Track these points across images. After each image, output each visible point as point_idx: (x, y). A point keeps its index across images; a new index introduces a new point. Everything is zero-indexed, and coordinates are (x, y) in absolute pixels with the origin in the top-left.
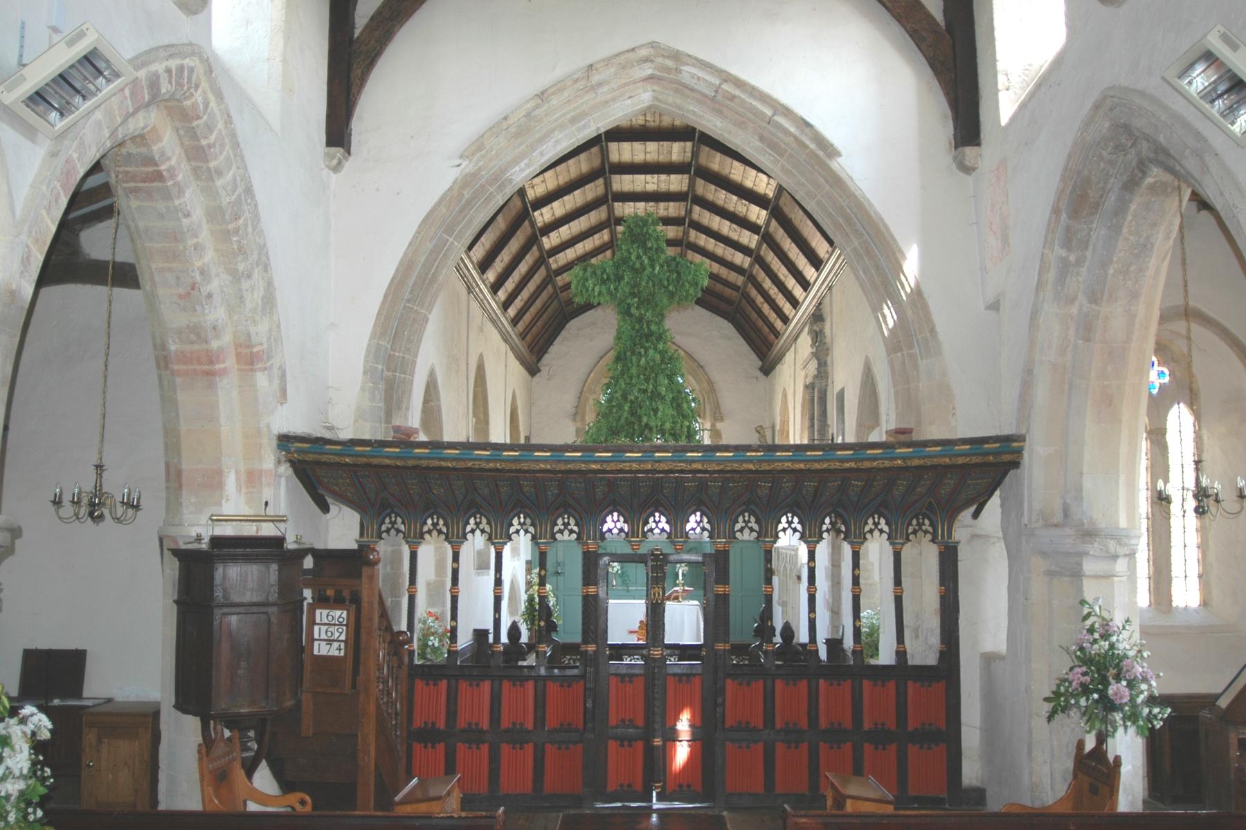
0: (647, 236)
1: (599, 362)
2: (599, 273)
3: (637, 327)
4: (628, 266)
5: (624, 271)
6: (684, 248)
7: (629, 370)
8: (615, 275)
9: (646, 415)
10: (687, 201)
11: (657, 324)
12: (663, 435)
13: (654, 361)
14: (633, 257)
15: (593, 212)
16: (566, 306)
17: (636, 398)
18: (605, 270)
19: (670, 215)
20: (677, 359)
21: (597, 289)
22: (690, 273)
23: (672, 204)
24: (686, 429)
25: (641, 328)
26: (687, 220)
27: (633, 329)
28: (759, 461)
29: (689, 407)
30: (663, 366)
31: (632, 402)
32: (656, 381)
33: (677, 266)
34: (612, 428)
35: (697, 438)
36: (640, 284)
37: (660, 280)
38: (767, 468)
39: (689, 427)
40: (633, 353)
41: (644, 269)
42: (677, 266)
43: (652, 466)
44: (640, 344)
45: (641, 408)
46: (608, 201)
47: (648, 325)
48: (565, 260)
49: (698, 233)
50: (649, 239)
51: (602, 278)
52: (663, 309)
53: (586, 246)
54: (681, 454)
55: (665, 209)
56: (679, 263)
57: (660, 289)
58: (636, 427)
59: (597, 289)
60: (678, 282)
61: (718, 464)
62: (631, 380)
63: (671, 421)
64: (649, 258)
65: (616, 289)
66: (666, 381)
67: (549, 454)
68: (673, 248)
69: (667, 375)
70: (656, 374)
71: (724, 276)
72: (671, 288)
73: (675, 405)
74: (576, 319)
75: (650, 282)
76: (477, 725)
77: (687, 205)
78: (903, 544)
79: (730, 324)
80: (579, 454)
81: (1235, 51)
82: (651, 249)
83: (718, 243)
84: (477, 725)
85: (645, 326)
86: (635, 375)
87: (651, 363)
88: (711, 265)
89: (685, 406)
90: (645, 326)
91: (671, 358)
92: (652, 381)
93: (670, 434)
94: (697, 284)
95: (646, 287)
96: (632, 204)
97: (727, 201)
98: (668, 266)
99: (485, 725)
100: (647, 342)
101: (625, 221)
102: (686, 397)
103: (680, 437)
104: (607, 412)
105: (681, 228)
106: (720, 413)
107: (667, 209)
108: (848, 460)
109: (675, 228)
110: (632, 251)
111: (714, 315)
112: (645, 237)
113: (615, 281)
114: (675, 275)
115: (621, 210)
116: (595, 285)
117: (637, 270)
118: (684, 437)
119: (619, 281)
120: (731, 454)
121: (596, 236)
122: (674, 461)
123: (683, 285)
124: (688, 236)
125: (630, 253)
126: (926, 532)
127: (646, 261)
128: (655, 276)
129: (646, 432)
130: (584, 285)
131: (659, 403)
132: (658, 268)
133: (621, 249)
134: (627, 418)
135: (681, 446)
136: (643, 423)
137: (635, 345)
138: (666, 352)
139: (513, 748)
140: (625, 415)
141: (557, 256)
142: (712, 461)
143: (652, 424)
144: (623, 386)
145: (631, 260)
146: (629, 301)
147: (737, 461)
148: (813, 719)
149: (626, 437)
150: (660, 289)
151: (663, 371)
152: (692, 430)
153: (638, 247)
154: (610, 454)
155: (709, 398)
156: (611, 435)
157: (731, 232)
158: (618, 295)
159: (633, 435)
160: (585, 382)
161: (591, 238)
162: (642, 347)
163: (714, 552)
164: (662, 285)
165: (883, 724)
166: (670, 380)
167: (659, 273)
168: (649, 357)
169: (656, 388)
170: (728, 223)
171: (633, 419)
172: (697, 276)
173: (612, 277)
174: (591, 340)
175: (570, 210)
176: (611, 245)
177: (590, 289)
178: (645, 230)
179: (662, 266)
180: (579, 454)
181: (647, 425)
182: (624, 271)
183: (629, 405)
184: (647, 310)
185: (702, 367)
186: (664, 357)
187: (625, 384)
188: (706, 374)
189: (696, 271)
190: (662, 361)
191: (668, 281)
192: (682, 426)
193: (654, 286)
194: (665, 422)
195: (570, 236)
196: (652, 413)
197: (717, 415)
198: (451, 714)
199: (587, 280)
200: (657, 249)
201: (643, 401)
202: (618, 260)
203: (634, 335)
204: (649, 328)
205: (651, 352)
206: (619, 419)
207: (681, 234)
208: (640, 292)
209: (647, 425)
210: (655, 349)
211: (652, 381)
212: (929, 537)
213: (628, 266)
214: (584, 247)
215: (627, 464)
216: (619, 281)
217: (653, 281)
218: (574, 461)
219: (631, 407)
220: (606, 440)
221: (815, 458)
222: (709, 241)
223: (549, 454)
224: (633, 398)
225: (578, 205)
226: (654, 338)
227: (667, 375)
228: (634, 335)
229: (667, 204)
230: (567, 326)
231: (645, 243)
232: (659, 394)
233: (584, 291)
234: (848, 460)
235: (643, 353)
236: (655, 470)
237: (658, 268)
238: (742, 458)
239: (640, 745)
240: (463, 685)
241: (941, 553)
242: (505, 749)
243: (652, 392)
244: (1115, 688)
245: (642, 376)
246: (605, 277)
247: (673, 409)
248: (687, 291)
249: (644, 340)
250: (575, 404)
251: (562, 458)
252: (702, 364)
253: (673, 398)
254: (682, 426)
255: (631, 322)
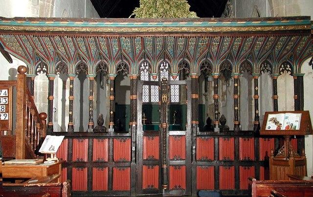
28: (214, 26)
38: (219, 30)
76: (82, 159)
78: (278, 76)
81: (308, 111)
84: (82, 159)
99: (86, 160)
108: (258, 27)
126: (288, 71)
139: (249, 158)
148: (237, 156)
163: (252, 129)
165: (249, 158)
198: (90, 155)
212: (289, 73)
221: (242, 25)
234: (258, 27)
239: (157, 167)
240: (76, 141)
241: (295, 80)
242: (95, 170)
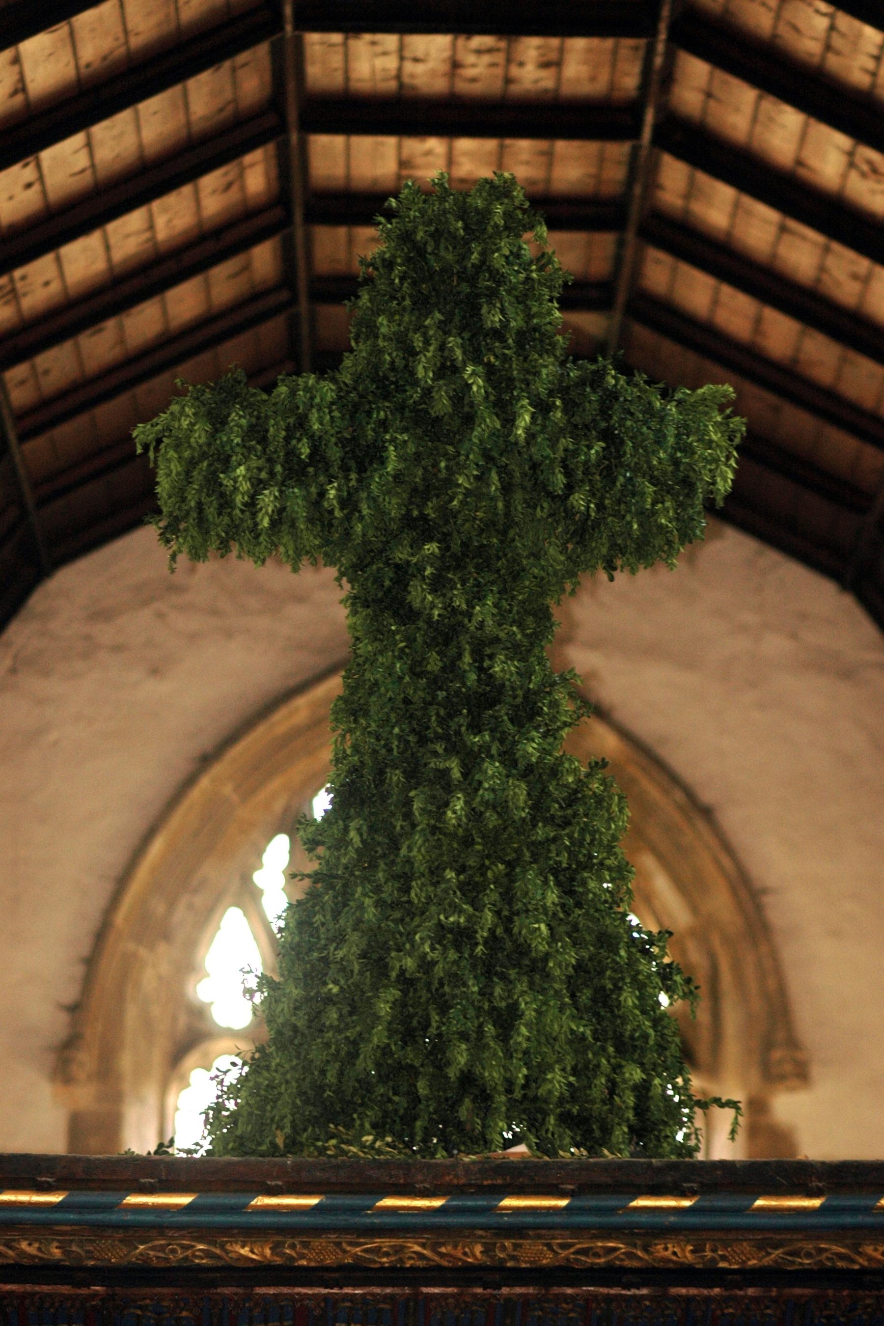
0: (485, 282)
1: (190, 781)
2: (276, 431)
3: (434, 663)
4: (401, 408)
5: (384, 425)
6: (630, 236)
7: (395, 846)
8: (342, 442)
9: (464, 1036)
10: (651, 33)
11: (517, 651)
12: (535, 1124)
13: (501, 807)
14: (423, 371)
15: (205, 77)
16: (42, 502)
17: (426, 965)
18: (302, 422)
19: (567, 90)
20: (599, 800)
21: (268, 500)
22: (660, 441)
23: (578, 44)
24: (631, 1100)
25: (451, 667)
26: (649, 117)
27: (416, 670)
29: (649, 1007)
30: (541, 832)
31: (406, 982)
32: (508, 896)
33: (604, 412)
34: (321, 1089)
35: (680, 1137)
36: (450, 482)
37: (535, 466)
39: (642, 1090)
40: (413, 775)
41: (469, 420)
42: (604, 412)
43: (488, 1250)
44: (446, 737)
45: (444, 1008)
46: (277, 23)
47: (478, 655)
48: (55, 287)
49: (702, 178)
50: (492, 295)
51: (291, 454)
52: (542, 588)
53: (161, 222)
54: (612, 1202)
55: (545, 65)
56: (613, 395)
57: (532, 505)
58: (422, 1087)
59: (268, 500)
60: (609, 475)
61: (762, 1246)
62: (407, 890)
63: (569, 1061)
64: (490, 373)
65: (348, 502)
66: (552, 897)
67: (55, 1198)
68: (578, 238)
69: (556, 871)
70: (510, 865)
71: (824, 375)
72: (579, 500)
73: (585, 996)
74: (85, 564)
75: (494, 476)
77: (650, 52)
79: (848, 602)
80: (185, 1200)
82: (498, 334)
83: (792, 224)
85: (467, 659)
86: (420, 866)
87: (492, 819)
88: (758, 321)
89: (629, 999)
90: (467, 659)
91: (574, 797)
92: (492, 895)
93: (565, 1119)
94: (688, 484)
95: (474, 495)
96: (390, 41)
97: (837, 42)
98: (570, 407)
100: (476, 728)
101: (390, 215)
102: (632, 962)
103: (607, 1131)
104: (301, 1023)
105: (619, 150)
106: (793, 1043)
107: (553, 64)
109: (592, 147)
110: (418, 342)
111: (772, 557)
112: (472, 281)
113: (346, 469)
114: (599, 446)
115: (336, 60)
116: (258, 485)
117: (438, 420)
118: (620, 1132)
119: (361, 470)
120: (816, 1203)
121: (210, 181)
122: (578, 1230)
123: (631, 491)
124: (652, 184)
125: (411, 352)
127: (478, 386)
128: (510, 447)
129: (465, 1110)
130: (212, 483)
131: (522, 986)
132: (525, 419)
133: (713, 1260)
134: (385, 1051)
135: (608, 1167)
136: (452, 1073)
137: (423, 741)
138: (554, 772)
140: (379, 1036)
141: (18, 273)
142: (737, 1229)
143: (493, 1074)
144: (371, 913)
145: (415, 383)
146: (401, 554)
147: (840, 1233)
149: (379, 1129)
150: (532, 505)
151: (539, 850)
152: (656, 1112)
153: (444, 328)
154: (313, 1201)
155: (737, 968)
156: (314, 1121)
157: (854, 176)
158: (359, 528)
159: (409, 1119)
160: (122, 881)
161: (187, 190)
162: (451, 751)
164: (541, 488)
166: (570, 893)
167: (531, 436)
168: (484, 794)
169: (508, 922)
170: (842, 140)
171: (411, 1057)
172: (688, 450)
173: (334, 453)
174: (155, 671)
175: (97, 65)
176: (277, 213)
177: (239, 499)
178: (475, 257)
179: (542, 408)
180: (185, 1200)
181: (468, 1079)
182: (384, 425)
183: (395, 993)
184: (477, 596)
185: (707, 813)
186: (544, 791)
187: (380, 904)
188: (727, 847)
189: (684, 429)
190: (538, 806)
191: (568, 473)
192: (613, 1088)
193: (507, 489)
194: (545, 1068)
195: (87, 179)
196: (489, 1029)
197: (777, 1054)
199: (225, 463)
200: (521, 335)
201: (456, 979)
202: (358, 378)
203: (418, 696)
204: (481, 670)
205: (492, 768)
206: (353, 1055)
207: (616, 174)
208: (447, 515)
209: (468, 1079)
210: (509, 759)
211: (492, 895)
213: (401, 408)
214: (151, 227)
215: (386, 1243)
216: (361, 470)
217: (503, 470)
218: (160, 1229)
219: (400, 1005)
220: (293, 1145)
222: (749, 213)
223: (55, 1198)
224: (410, 963)
225: (136, 42)
226: (503, 711)
227: (556, 871)
228: (418, 696)
229: (555, 42)
230: (37, 601)
231: (475, 309)
232: (522, 950)
233: (211, 512)
235: (456, 774)
236: (501, 1268)
237: (525, 419)
238: (860, 1219)
243: (492, 940)
244: (607, 981)
245: (450, 874)
246: (305, 451)
247: (580, 1012)
248: (646, 517)
249: (462, 720)
250: (70, 994)
251: (114, 1217)
252: (707, 796)
253: (579, 967)
254: (613, 1088)
255: (410, 640)
